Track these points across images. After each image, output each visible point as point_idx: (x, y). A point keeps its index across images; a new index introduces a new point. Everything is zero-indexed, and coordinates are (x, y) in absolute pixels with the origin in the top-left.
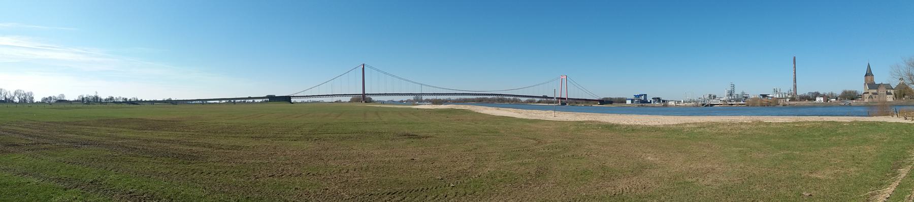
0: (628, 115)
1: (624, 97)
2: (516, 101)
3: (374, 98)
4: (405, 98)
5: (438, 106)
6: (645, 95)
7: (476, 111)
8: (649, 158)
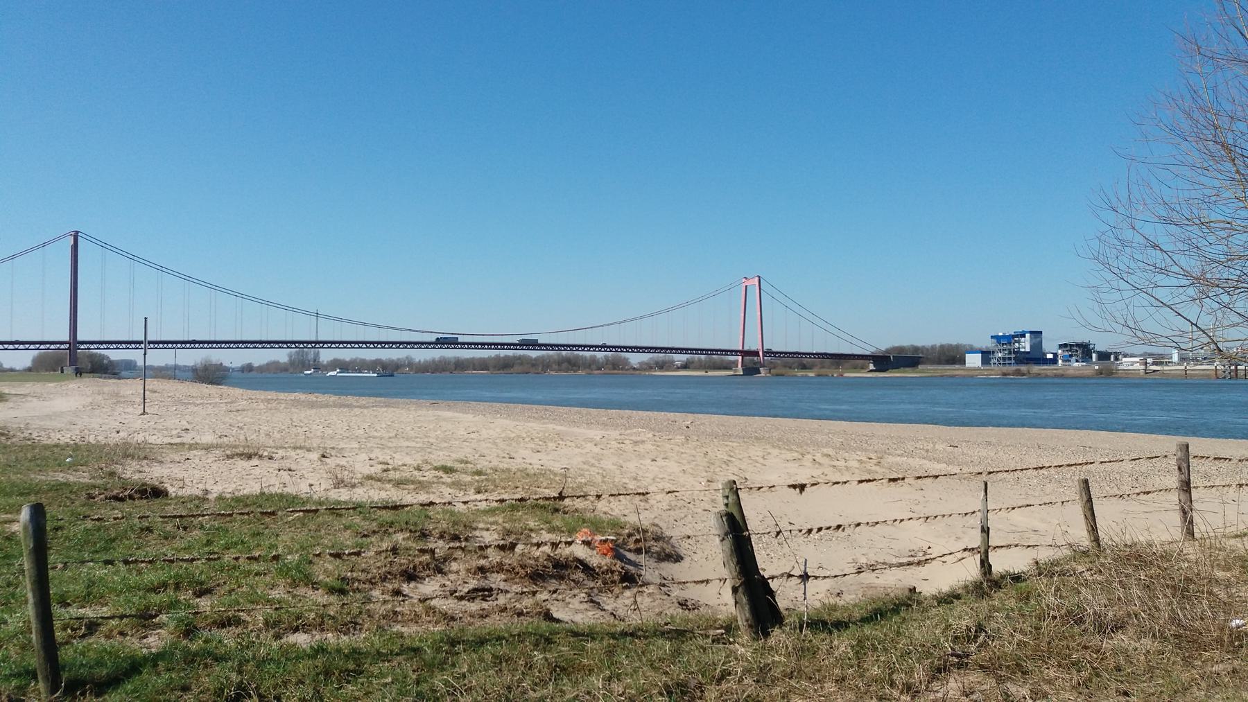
2: (616, 365)
4: (259, 357)
6: (1036, 334)
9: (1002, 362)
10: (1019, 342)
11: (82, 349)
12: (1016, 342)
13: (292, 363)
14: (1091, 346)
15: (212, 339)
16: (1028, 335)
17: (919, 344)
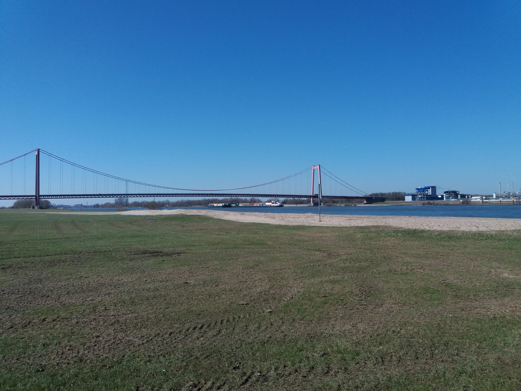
0: (395, 217)
1: (465, 194)
3: (53, 202)
5: (446, 228)
6: (434, 188)
7: (216, 217)
8: (506, 275)
9: (420, 199)
10: (427, 191)
11: (25, 199)
12: (426, 191)
13: (116, 203)
14: (457, 192)
15: (61, 194)
16: (431, 188)
17: (383, 192)
